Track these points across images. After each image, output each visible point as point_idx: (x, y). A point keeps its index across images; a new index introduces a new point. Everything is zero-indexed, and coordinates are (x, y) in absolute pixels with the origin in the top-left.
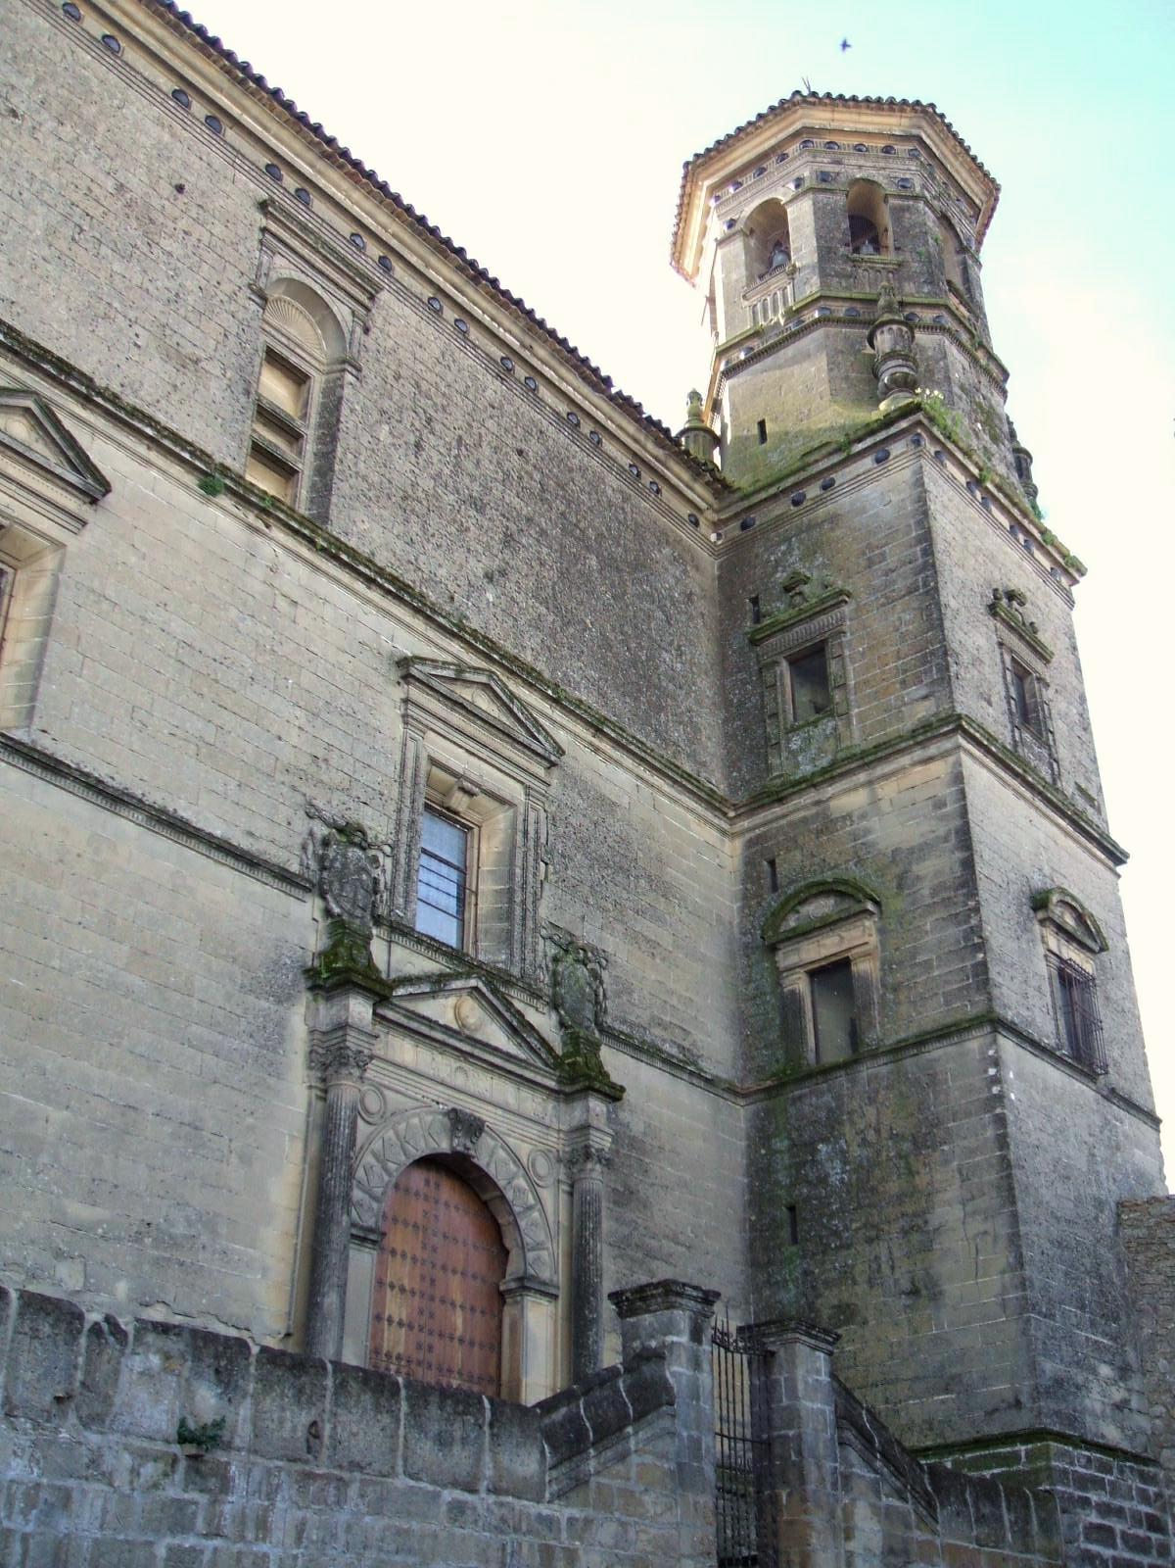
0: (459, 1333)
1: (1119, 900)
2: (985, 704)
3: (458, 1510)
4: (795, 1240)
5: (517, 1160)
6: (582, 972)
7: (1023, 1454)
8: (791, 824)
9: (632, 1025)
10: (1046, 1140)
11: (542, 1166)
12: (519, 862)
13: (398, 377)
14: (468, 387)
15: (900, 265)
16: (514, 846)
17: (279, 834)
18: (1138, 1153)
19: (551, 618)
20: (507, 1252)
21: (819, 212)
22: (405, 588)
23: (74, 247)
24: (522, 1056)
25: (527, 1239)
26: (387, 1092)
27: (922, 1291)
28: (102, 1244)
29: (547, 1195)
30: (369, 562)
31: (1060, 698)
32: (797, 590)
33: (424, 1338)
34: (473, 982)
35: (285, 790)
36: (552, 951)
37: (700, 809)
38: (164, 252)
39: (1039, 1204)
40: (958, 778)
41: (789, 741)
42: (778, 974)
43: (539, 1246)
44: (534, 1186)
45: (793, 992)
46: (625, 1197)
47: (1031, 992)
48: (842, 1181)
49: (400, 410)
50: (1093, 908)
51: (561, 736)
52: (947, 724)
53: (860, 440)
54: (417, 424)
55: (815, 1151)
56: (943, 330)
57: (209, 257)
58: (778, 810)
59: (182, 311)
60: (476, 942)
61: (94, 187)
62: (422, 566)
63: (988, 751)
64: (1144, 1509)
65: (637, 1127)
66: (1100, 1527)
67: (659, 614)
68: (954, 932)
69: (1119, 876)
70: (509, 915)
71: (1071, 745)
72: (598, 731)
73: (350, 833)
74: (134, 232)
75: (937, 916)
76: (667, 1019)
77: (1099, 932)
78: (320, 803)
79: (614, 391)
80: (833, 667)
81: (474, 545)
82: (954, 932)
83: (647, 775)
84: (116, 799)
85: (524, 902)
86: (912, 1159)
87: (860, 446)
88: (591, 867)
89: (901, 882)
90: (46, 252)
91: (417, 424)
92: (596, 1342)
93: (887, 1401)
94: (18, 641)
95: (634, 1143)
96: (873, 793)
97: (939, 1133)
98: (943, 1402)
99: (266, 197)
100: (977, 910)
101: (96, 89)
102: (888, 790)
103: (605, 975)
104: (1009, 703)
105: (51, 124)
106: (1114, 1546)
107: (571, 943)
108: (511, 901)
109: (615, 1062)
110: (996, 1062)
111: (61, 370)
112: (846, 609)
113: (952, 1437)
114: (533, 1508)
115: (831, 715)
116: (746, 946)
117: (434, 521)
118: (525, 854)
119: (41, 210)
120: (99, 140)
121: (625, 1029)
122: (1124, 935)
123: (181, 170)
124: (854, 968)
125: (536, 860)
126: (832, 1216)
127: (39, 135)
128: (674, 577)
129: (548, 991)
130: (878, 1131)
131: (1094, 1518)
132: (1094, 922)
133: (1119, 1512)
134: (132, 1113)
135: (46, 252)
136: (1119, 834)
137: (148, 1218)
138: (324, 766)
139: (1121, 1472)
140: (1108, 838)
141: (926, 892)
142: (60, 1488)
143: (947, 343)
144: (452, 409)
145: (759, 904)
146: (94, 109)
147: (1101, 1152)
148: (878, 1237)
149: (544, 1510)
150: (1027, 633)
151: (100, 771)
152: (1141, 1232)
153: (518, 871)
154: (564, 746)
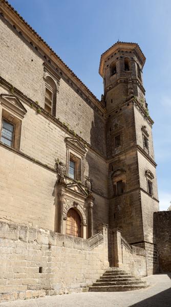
3: (80, 252)
21: (121, 64)
40: (137, 154)
65: (96, 203)
73: (61, 163)
74: (27, 68)
80: (121, 138)
102: (128, 156)
131: (149, 252)
150: (146, 132)
151: (28, 155)
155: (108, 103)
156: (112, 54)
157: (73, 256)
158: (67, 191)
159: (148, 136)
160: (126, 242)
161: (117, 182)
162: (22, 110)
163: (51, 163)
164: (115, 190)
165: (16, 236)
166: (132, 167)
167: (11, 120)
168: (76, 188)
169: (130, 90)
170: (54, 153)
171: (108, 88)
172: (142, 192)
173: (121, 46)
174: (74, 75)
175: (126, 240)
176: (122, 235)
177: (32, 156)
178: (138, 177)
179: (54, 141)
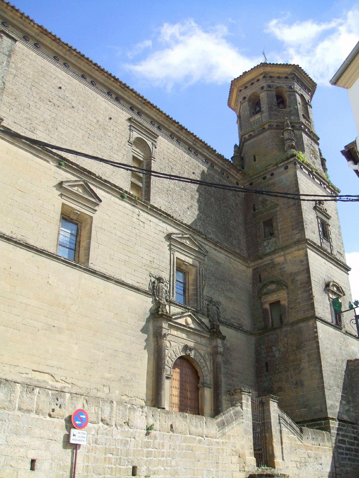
0: (189, 397)
1: (348, 281)
2: (313, 234)
3: (200, 441)
4: (267, 371)
5: (201, 355)
6: (214, 308)
7: (323, 423)
8: (264, 265)
9: (226, 319)
10: (329, 346)
11: (207, 357)
12: (198, 281)
13: (164, 158)
14: (181, 157)
15: (290, 111)
16: (197, 277)
17: (144, 282)
18: (353, 347)
19: (203, 217)
20: (199, 377)
21: (268, 97)
22: (169, 215)
23: (89, 139)
24: (201, 330)
25: (204, 374)
26: (171, 342)
27: (299, 384)
28: (112, 382)
29: (208, 363)
30: (160, 210)
31: (333, 228)
32: (265, 203)
33: (68, 324)
34: (190, 313)
35: (145, 270)
36: (207, 303)
37: (241, 262)
38: (109, 136)
39: (327, 362)
40: (306, 255)
41: (263, 243)
42: (262, 304)
43: (207, 376)
44: (205, 361)
45: (266, 309)
46: (226, 362)
47: (325, 309)
48: (279, 356)
49: (165, 167)
50: (341, 284)
51: (207, 247)
52: (304, 241)
53: (280, 163)
54: (169, 170)
55: (272, 349)
57: (119, 135)
58: (261, 261)
59: (114, 151)
60: (189, 302)
61: (92, 122)
62: (173, 208)
63: (314, 247)
64: (353, 435)
66: (342, 440)
67: (230, 211)
68: (306, 295)
69: (348, 274)
70: (196, 295)
71: (336, 240)
72: (216, 245)
73: (160, 279)
75: (302, 290)
76: (235, 317)
78: (152, 273)
80: (274, 224)
81: (184, 200)
82: (306, 295)
83: (228, 255)
84: (107, 278)
85: (200, 291)
86: (296, 351)
87: (281, 165)
88: (216, 280)
89: (293, 281)
90: (83, 142)
91: (169, 170)
92: (221, 398)
93: (290, 410)
94: (84, 241)
95: (228, 349)
96: (285, 257)
97: (303, 345)
98: (304, 411)
99: (131, 117)
101: (90, 96)
102: (289, 257)
103: (220, 307)
104: (319, 232)
105: (81, 108)
106: (345, 444)
107: (211, 300)
108: (197, 291)
109: (223, 329)
111: (89, 173)
113: (306, 419)
114: (215, 440)
115: (274, 237)
116: (254, 296)
117: (174, 196)
118: (200, 279)
119: (81, 131)
120: (92, 110)
121: (225, 320)
122: (350, 290)
123: (111, 113)
124: (281, 303)
125: (202, 280)
126: (276, 365)
127: (79, 112)
128: (233, 200)
129: (206, 313)
130: (287, 344)
133: (347, 436)
134: (116, 352)
135: (83, 142)
136: (349, 264)
137: (122, 376)
138: (153, 263)
139: (347, 427)
140: (346, 265)
141: (299, 284)
142: (126, 440)
144: (177, 164)
145: (257, 285)
146: (90, 101)
147: (343, 348)
148: (288, 370)
149: (217, 440)
150: (324, 213)
151: (103, 271)
152: (353, 367)
153: (198, 284)
154: (208, 251)
155: (247, 160)
156: (253, 79)
157: (188, 448)
158: (171, 326)
159: (328, 217)
160: (289, 421)
161: (270, 304)
162: (93, 200)
163: (142, 281)
164: (265, 319)
165: (97, 418)
166: (298, 278)
167: (75, 218)
168: (189, 320)
169: (288, 143)
170: (148, 263)
171: (247, 136)
172: (319, 324)
173: (268, 69)
174: (182, 128)
175: (288, 415)
176: (280, 406)
177: (109, 272)
178: (310, 297)
179: (148, 242)
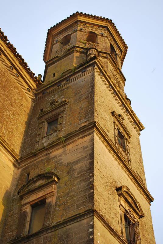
32: (54, 104)
40: (93, 140)
56: (107, 58)
69: (150, 205)
77: (141, 208)
79: (8, 42)
82: (85, 184)
100: (93, 176)
110: (92, 227)
112: (67, 106)
132: (140, 206)
141: (76, 173)
143: (108, 61)
